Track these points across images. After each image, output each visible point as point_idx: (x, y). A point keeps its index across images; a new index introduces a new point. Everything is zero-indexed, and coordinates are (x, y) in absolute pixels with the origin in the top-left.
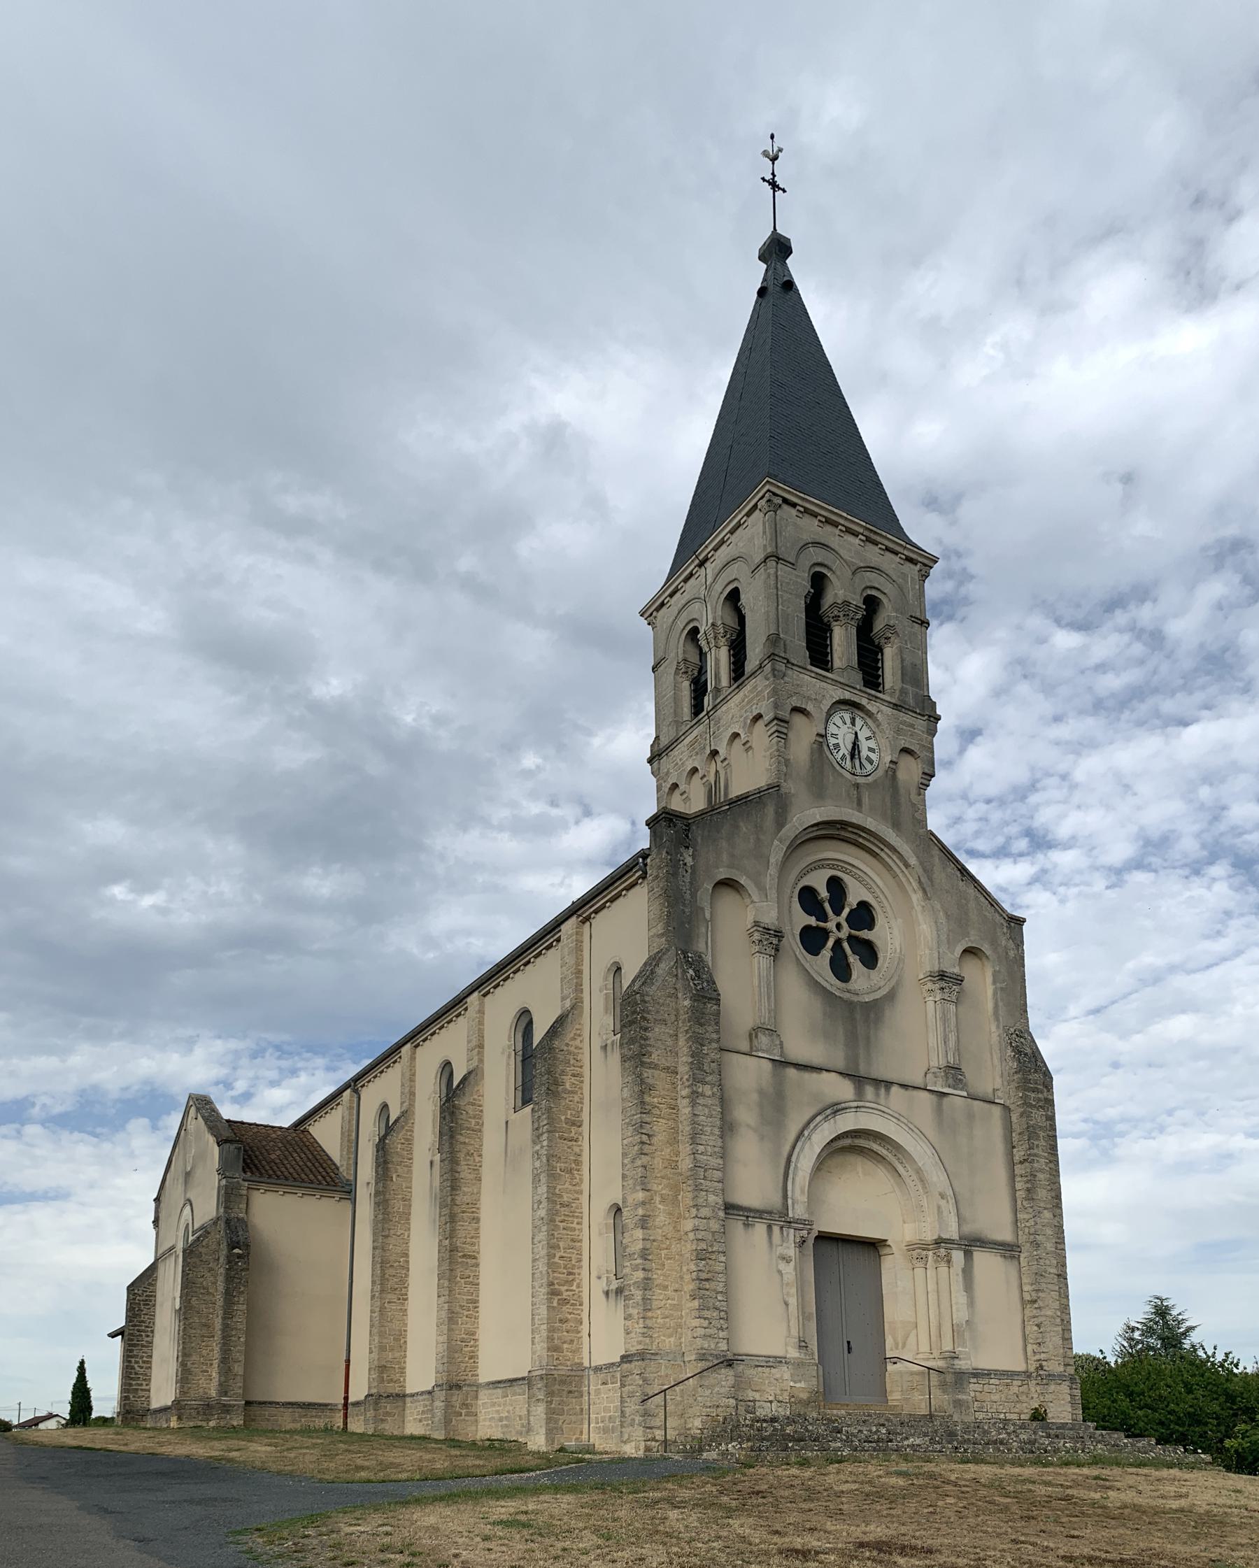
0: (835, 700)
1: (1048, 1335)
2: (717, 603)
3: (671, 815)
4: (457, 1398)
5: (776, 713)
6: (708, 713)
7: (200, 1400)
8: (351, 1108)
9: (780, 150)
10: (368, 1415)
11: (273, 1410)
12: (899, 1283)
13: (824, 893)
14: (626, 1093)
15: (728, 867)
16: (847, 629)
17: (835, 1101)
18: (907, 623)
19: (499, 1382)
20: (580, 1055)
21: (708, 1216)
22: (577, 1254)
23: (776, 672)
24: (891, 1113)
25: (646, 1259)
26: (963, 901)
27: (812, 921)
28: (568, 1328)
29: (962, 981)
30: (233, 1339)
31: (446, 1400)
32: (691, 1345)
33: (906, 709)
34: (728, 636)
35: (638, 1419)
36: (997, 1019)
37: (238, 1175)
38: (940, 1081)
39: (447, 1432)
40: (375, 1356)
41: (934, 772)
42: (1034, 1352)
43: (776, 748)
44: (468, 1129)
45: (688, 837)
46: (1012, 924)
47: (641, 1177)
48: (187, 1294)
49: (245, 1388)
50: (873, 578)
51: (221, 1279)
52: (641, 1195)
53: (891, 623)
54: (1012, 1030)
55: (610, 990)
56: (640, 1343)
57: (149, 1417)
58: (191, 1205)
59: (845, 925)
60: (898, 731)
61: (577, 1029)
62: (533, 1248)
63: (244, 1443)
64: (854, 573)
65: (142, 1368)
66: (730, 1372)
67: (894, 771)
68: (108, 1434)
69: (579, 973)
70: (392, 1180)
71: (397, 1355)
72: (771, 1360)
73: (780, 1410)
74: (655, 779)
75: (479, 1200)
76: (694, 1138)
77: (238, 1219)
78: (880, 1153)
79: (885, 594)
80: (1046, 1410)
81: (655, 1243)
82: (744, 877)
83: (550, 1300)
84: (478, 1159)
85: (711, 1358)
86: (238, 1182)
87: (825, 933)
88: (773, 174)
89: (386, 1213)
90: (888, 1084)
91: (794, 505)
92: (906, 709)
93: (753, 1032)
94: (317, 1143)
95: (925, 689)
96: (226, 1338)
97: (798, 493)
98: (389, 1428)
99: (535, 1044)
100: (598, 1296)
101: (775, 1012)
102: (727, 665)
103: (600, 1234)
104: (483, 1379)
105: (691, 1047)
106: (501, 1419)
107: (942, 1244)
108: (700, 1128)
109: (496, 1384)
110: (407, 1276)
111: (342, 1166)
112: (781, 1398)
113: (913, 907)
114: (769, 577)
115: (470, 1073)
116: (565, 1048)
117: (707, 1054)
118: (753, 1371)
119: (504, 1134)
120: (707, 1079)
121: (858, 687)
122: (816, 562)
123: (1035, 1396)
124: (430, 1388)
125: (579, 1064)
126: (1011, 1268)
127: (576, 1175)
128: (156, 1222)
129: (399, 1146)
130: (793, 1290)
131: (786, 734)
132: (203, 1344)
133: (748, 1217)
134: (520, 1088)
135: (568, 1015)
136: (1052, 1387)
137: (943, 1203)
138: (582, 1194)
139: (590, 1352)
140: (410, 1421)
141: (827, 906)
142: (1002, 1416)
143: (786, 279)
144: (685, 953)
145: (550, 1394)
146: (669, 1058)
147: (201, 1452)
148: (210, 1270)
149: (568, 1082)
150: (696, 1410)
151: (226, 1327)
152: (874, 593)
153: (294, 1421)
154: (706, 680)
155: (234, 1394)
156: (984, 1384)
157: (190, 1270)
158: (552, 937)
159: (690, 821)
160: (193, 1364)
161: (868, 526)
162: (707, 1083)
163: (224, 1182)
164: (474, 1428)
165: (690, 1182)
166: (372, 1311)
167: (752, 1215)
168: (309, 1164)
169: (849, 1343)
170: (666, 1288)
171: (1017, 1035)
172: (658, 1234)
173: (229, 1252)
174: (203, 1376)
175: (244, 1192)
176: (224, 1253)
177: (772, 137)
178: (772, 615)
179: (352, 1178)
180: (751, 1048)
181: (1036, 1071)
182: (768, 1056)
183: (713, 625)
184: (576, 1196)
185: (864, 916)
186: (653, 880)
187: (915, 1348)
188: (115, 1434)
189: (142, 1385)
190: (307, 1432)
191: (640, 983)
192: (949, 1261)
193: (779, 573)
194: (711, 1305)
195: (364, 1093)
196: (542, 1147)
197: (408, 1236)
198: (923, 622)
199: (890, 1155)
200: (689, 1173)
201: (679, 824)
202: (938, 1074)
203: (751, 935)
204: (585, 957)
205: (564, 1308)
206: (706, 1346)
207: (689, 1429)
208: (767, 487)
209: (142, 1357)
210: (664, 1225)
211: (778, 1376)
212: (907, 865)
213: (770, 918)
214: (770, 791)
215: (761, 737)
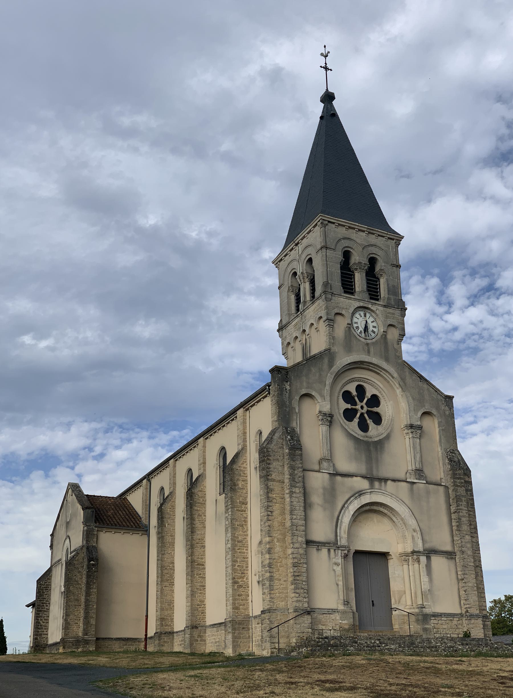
0: (355, 307)
1: (470, 596)
2: (303, 263)
3: (279, 368)
4: (196, 633)
5: (327, 317)
6: (301, 312)
7: (74, 638)
8: (146, 489)
9: (329, 52)
10: (156, 643)
11: (110, 643)
12: (396, 572)
13: (354, 393)
14: (262, 493)
15: (306, 388)
16: (361, 274)
17: (360, 489)
18: (390, 267)
19: (215, 624)
20: (246, 471)
21: (298, 547)
22: (246, 564)
23: (327, 299)
24: (387, 493)
25: (270, 568)
26: (421, 391)
27: (349, 406)
28: (242, 598)
29: (422, 428)
30: (90, 606)
31: (191, 634)
32: (291, 605)
33: (390, 307)
34: (309, 278)
35: (268, 639)
36: (441, 446)
37: (93, 525)
38: (413, 476)
39: (191, 649)
40: (159, 613)
41: (405, 334)
42: (464, 604)
43: (328, 332)
44: (199, 503)
45: (287, 377)
46: (447, 399)
47: (268, 531)
48: (68, 585)
49: (97, 631)
50: (373, 250)
51: (84, 576)
52: (268, 539)
53: (382, 268)
54: (448, 450)
55: (258, 442)
56: (268, 605)
57: (47, 648)
58: (69, 539)
59: (365, 406)
60: (387, 317)
61: (244, 459)
62: (226, 562)
63: (96, 657)
64: (363, 249)
65: (44, 623)
66: (309, 617)
67: (386, 336)
68: (30, 656)
69: (245, 433)
70: (165, 527)
71: (169, 612)
72: (330, 611)
73: (335, 634)
74: (281, 339)
75: (205, 537)
76: (291, 513)
77: (93, 546)
78: (383, 512)
79: (379, 256)
80: (470, 632)
81: (275, 560)
82: (314, 392)
83: (233, 586)
84: (204, 517)
85: (300, 611)
86: (92, 528)
87: (356, 411)
88: (326, 64)
89: (163, 543)
90: (386, 480)
91: (334, 223)
92: (390, 307)
93: (321, 461)
94: (131, 505)
95: (400, 295)
96: (87, 606)
97: (335, 218)
98: (166, 649)
99: (228, 463)
100: (255, 584)
101: (331, 450)
102: (309, 291)
103: (256, 555)
104: (208, 623)
105: (289, 471)
106: (216, 643)
107: (415, 554)
108: (294, 507)
109: (214, 625)
110: (173, 573)
111: (143, 517)
112: (335, 628)
113: (397, 396)
114: (323, 256)
115: (199, 476)
116: (239, 469)
117: (297, 474)
118: (321, 616)
119: (215, 506)
120: (297, 485)
121: (366, 300)
122: (345, 246)
123: (465, 625)
124: (183, 629)
125: (246, 475)
126: (452, 563)
127: (245, 527)
128: (51, 547)
129: (169, 510)
130: (341, 578)
131: (333, 326)
132: (76, 609)
133: (318, 546)
134: (222, 484)
135: (240, 453)
136: (473, 621)
137: (415, 534)
138: (248, 536)
139: (252, 610)
140: (176, 645)
141: (356, 398)
142: (449, 635)
143: (332, 112)
144: (286, 428)
145: (234, 629)
146: (280, 476)
147: (76, 662)
148: (79, 572)
149: (240, 484)
150: (293, 634)
151: (87, 601)
152: (373, 256)
153: (120, 647)
154: (300, 296)
155: (91, 634)
156: (438, 620)
157: (69, 572)
158: (234, 416)
159: (288, 370)
160: (70, 620)
161: (369, 227)
162: (297, 487)
163: (86, 528)
164: (204, 647)
165: (290, 532)
166: (157, 591)
167: (320, 545)
168: (127, 517)
169: (373, 601)
170: (280, 580)
171: (451, 452)
172: (276, 556)
173: (88, 563)
174: (75, 625)
175: (96, 533)
176: (86, 563)
177: (325, 47)
178: (325, 273)
179: (147, 524)
180: (320, 468)
181: (460, 469)
182: (327, 472)
183: (302, 273)
184: (245, 537)
185: (375, 401)
186: (273, 397)
187: (405, 603)
188: (33, 656)
189: (44, 631)
190: (126, 652)
191: (266, 443)
192: (419, 562)
193: (327, 254)
194: (300, 587)
195: (153, 481)
196: (229, 515)
197: (174, 554)
198: (397, 266)
199: (389, 513)
200: (289, 528)
201: (283, 372)
202: (411, 473)
203: (318, 417)
204: (247, 425)
205: (240, 589)
206: (298, 605)
207: (291, 643)
208: (320, 218)
209: (44, 617)
210: (279, 552)
211: (333, 618)
212: (393, 377)
213: (326, 408)
214: (326, 352)
215: (322, 326)
